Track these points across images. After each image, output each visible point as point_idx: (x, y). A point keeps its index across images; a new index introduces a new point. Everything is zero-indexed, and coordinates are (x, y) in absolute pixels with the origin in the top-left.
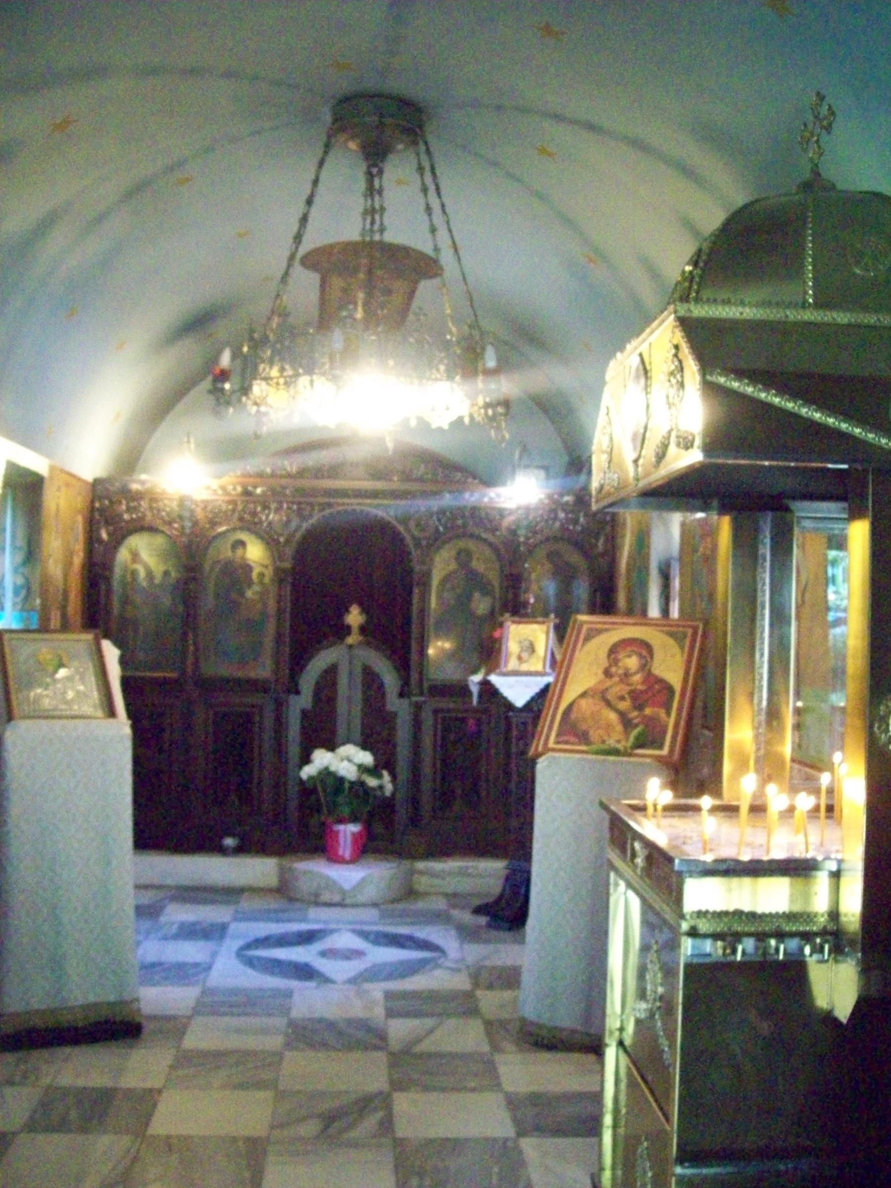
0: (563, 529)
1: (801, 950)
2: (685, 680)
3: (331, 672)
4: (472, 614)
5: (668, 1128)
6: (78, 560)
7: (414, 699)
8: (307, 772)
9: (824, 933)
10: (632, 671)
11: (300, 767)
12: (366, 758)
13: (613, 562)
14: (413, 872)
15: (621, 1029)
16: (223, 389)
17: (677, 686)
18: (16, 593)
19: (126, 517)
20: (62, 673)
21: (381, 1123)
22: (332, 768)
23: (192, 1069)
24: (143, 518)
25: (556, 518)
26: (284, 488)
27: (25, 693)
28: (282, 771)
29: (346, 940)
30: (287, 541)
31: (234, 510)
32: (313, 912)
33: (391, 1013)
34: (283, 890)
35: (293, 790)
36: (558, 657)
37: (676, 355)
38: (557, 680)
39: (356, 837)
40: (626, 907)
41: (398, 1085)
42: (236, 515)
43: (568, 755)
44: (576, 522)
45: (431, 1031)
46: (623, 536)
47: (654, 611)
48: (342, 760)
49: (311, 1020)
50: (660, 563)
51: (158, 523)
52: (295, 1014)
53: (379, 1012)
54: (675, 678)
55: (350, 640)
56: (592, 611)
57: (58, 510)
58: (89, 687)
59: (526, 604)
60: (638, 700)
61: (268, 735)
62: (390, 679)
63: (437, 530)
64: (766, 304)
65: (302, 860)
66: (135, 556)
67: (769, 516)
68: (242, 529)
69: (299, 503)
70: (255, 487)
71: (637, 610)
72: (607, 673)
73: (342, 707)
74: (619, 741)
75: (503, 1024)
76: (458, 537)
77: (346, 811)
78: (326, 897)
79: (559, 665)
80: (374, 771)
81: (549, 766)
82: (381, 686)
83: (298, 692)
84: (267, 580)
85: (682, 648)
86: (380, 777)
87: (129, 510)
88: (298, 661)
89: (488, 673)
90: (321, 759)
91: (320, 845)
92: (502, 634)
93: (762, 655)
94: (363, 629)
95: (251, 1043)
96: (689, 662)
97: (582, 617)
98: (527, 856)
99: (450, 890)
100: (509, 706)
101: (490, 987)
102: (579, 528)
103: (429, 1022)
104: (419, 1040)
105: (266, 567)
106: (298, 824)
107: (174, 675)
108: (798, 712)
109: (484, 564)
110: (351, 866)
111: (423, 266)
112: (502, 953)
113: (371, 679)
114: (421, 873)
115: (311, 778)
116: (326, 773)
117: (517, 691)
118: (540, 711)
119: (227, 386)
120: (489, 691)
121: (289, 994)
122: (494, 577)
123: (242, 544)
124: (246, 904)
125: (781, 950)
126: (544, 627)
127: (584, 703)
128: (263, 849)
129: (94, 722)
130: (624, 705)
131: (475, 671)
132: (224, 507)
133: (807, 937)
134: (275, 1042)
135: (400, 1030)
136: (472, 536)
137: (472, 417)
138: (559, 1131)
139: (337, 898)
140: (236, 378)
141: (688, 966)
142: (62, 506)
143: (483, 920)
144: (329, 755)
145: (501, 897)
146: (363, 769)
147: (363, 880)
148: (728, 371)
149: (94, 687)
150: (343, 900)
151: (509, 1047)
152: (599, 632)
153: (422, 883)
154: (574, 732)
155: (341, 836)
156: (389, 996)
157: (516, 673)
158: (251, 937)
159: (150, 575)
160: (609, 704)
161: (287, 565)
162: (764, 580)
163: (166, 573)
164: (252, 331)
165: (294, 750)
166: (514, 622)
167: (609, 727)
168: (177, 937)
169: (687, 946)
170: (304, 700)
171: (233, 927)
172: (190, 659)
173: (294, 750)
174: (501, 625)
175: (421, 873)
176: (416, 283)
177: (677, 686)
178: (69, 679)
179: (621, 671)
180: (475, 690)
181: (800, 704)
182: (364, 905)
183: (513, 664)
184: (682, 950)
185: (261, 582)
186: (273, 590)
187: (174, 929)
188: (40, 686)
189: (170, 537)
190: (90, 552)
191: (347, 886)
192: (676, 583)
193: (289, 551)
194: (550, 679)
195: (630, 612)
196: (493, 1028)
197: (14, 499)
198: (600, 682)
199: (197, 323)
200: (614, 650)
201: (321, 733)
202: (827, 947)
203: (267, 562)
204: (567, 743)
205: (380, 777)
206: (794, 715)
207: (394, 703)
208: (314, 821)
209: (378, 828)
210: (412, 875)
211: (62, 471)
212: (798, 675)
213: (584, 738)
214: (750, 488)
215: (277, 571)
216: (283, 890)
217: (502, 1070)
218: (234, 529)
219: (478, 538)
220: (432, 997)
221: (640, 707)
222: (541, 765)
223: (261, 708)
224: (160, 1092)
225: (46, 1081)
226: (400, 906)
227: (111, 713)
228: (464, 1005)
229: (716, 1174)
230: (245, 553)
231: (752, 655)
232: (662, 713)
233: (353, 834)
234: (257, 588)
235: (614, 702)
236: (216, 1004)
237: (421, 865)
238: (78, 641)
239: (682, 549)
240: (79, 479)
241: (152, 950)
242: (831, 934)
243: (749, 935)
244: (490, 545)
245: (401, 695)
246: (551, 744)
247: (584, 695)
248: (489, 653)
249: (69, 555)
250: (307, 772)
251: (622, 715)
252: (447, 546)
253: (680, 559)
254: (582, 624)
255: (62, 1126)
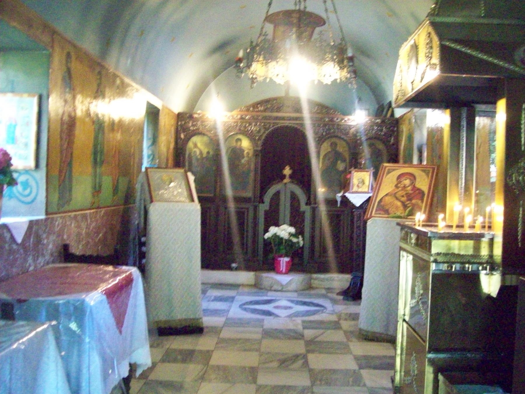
0: (376, 134)
1: (478, 268)
2: (430, 188)
3: (278, 194)
4: (337, 170)
5: (424, 344)
6: (172, 146)
7: (312, 206)
8: (267, 235)
9: (487, 263)
10: (407, 186)
11: (264, 234)
12: (292, 230)
13: (397, 149)
14: (311, 279)
15: (404, 315)
16: (240, 66)
17: (426, 192)
18: (149, 157)
19: (192, 128)
20: (172, 184)
21: (304, 363)
22: (278, 234)
23: (262, 259)
24: (198, 129)
25: (373, 129)
26: (258, 116)
27: (157, 193)
28: (255, 234)
29: (284, 303)
30: (259, 139)
31: (237, 126)
32: (270, 293)
33: (304, 328)
34: (257, 286)
35: (261, 241)
36: (374, 186)
37: (429, 36)
38: (374, 194)
39: (287, 263)
40: (406, 263)
41: (308, 351)
42: (238, 128)
43: (381, 219)
44: (381, 130)
45: (322, 334)
46: (402, 141)
47: (415, 161)
48: (282, 230)
49: (272, 329)
50: (418, 146)
51: (204, 131)
52: (264, 327)
53: (300, 327)
54: (425, 187)
55: (285, 181)
56: (389, 162)
57: (165, 125)
58: (182, 190)
59: (361, 164)
60: (410, 197)
61: (251, 220)
62: (302, 197)
63: (322, 134)
64: (464, 16)
65: (265, 273)
66: (196, 145)
67: (466, 108)
68: (240, 133)
69: (265, 123)
70: (246, 116)
71: (408, 160)
72: (397, 186)
73: (282, 208)
74: (401, 213)
75: (352, 332)
76: (331, 137)
77: (284, 251)
78: (275, 287)
79: (376, 186)
80: (296, 235)
81: (372, 223)
82: (298, 201)
83: (263, 202)
84: (250, 155)
85: (428, 176)
86: (298, 238)
87: (193, 125)
88: (263, 190)
89: (344, 193)
90: (273, 230)
91: (272, 266)
92: (350, 176)
93: (462, 165)
94: (291, 177)
95: (247, 336)
96: (431, 181)
97: (386, 164)
98: (362, 270)
99: (326, 287)
100: (353, 206)
101: (346, 319)
102: (383, 133)
103: (321, 331)
104: (316, 337)
105: (250, 150)
106: (264, 258)
107: (212, 195)
108: (477, 195)
109: (342, 148)
110: (286, 275)
111: (319, 21)
112: (352, 308)
113: (294, 198)
114: (316, 279)
115: (268, 238)
116: (275, 236)
117: (357, 200)
118: (366, 209)
119: (242, 65)
120: (345, 201)
121: (263, 320)
122: (347, 155)
123: (239, 140)
124: (241, 289)
125: (469, 267)
126: (368, 173)
127: (387, 198)
128: (248, 268)
129: (186, 204)
130: (404, 199)
131: (340, 192)
132: (232, 124)
133: (481, 264)
134: (259, 336)
135: (309, 333)
136: (336, 137)
137: (341, 80)
138: (375, 368)
139: (280, 288)
140: (245, 61)
141: (434, 275)
142: (166, 122)
143: (341, 297)
144: (277, 228)
145: (348, 288)
146: (291, 235)
147: (290, 281)
148: (449, 40)
149: (185, 190)
150: (282, 289)
151: (354, 339)
152: (394, 170)
153: (315, 283)
154: (384, 209)
155: (281, 262)
156: (303, 322)
157: (357, 192)
158: (244, 302)
159: (201, 153)
160: (397, 199)
161: (259, 148)
162: (462, 173)
163: (208, 153)
164: (252, 42)
165: (261, 227)
166: (356, 171)
167: (397, 208)
168: (213, 301)
169: (433, 266)
170: (263, 208)
171: (237, 297)
172: (218, 190)
173: (261, 227)
174: (350, 172)
175: (316, 279)
176: (315, 28)
177: (426, 192)
178: (175, 187)
179: (402, 186)
180: (339, 200)
181: (478, 192)
182: (291, 291)
183: (355, 189)
184: (431, 269)
185: (248, 156)
186: (253, 160)
187: (213, 298)
188: (164, 189)
189: (209, 137)
190: (176, 143)
191: (284, 283)
192: (425, 154)
193: (260, 143)
194: (371, 195)
195: (405, 162)
196: (348, 334)
197: (148, 121)
198: (394, 190)
199: (221, 47)
200: (400, 177)
201: (273, 219)
202: (488, 267)
203: (251, 148)
204: (380, 214)
205: (298, 238)
206: (475, 203)
207: (304, 207)
208: (271, 256)
209: (296, 260)
210: (310, 280)
211: (167, 108)
212: (477, 182)
213: (387, 212)
214: (458, 98)
215: (255, 151)
216: (257, 286)
217: (351, 347)
218: (237, 134)
219: (340, 138)
220: (321, 322)
221: (410, 200)
222: (369, 223)
223: (248, 209)
224: (212, 351)
225: (167, 347)
226: (307, 292)
227: (192, 200)
228: (336, 326)
229: (444, 358)
230: (241, 144)
231: (458, 164)
232: (420, 202)
233: (286, 262)
234: (246, 159)
235: (400, 198)
236: (232, 323)
237: (315, 276)
238: (177, 172)
239: (428, 139)
240: (173, 112)
241: (205, 305)
242: (490, 263)
243: (458, 263)
244: (345, 140)
245: (307, 204)
246: (373, 215)
247: (387, 195)
248: (345, 185)
249: (169, 143)
250: (267, 235)
251: (403, 203)
252: (327, 141)
253: (427, 144)
254: (386, 167)
255: (175, 361)
